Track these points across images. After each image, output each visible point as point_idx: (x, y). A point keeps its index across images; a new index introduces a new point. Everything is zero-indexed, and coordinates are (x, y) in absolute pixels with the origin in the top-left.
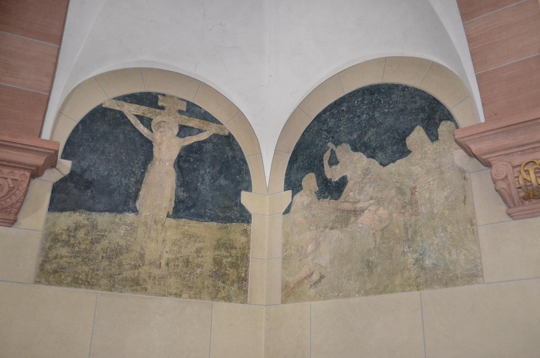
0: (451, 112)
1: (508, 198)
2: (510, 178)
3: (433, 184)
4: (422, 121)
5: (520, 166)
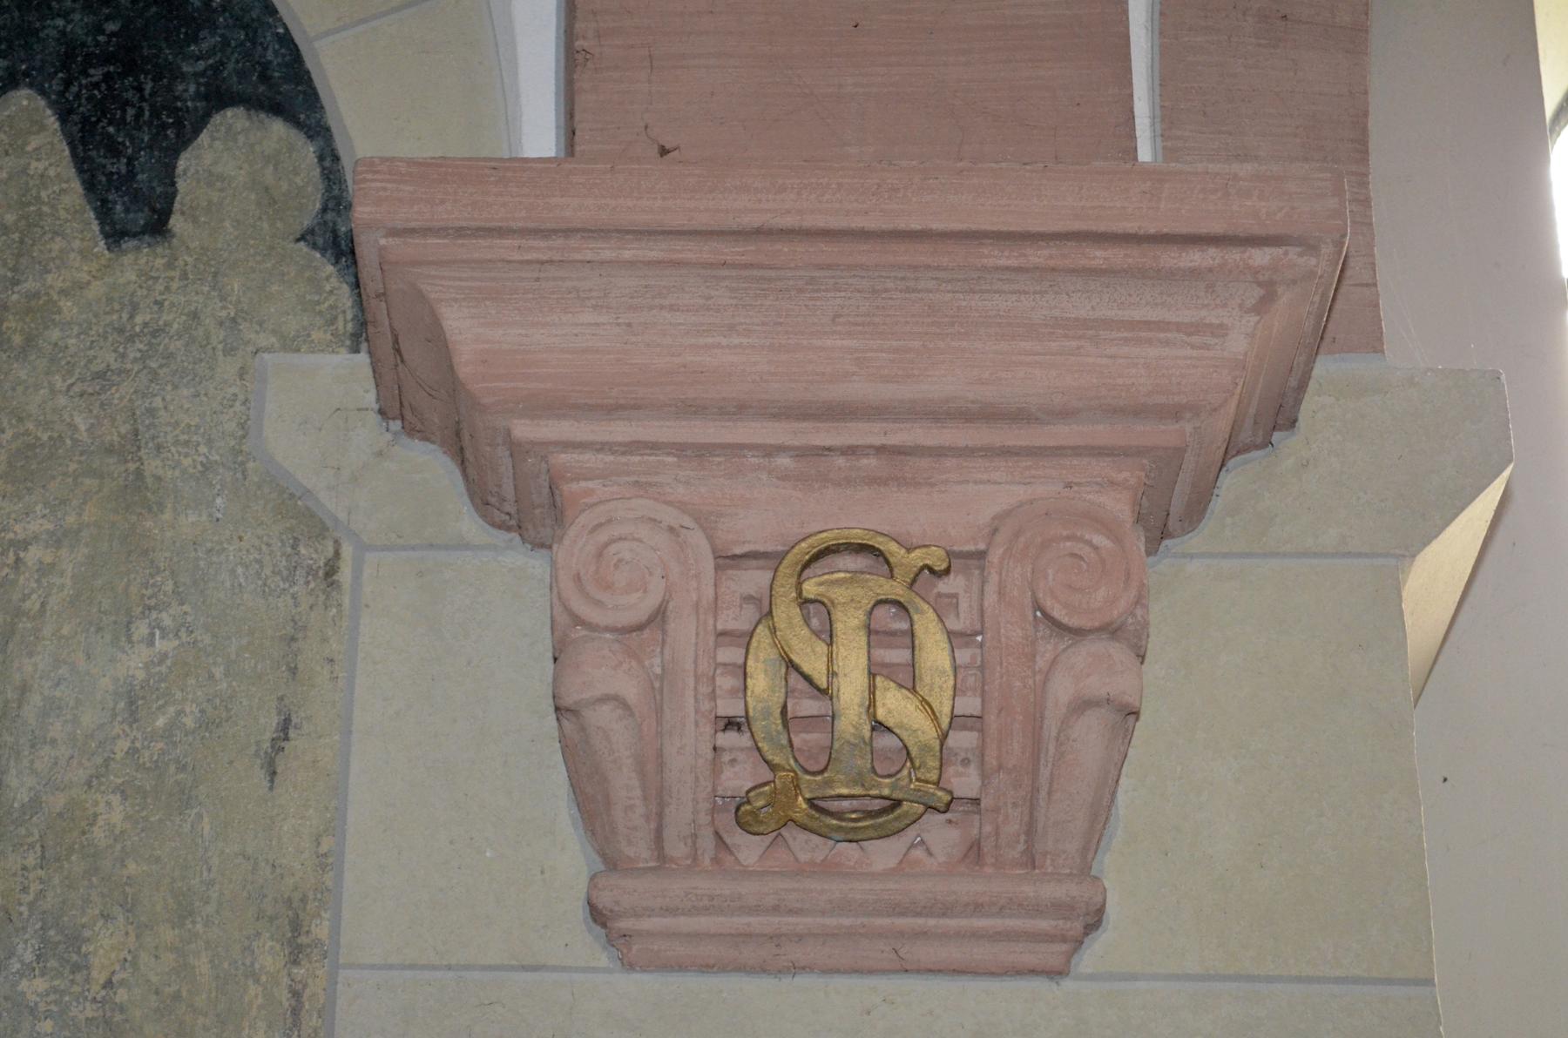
0: (309, 64)
1: (625, 785)
2: (684, 631)
3: (44, 570)
4: (66, 61)
5: (772, 559)
